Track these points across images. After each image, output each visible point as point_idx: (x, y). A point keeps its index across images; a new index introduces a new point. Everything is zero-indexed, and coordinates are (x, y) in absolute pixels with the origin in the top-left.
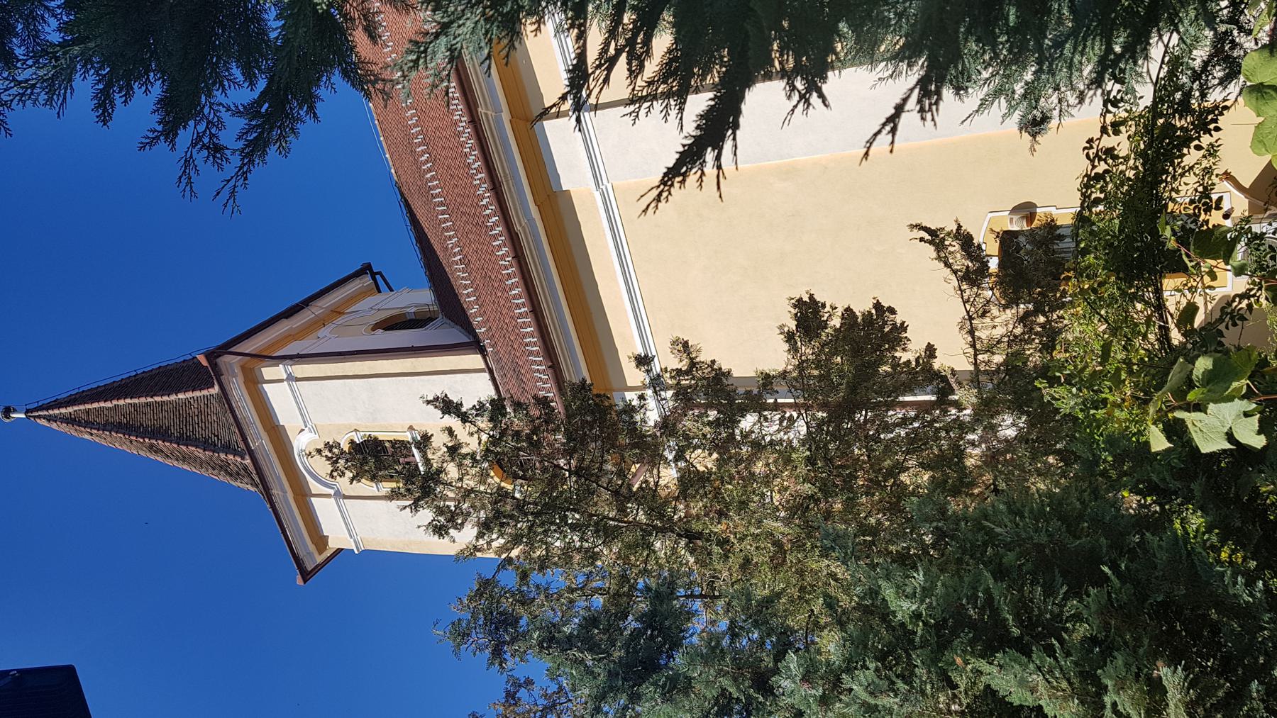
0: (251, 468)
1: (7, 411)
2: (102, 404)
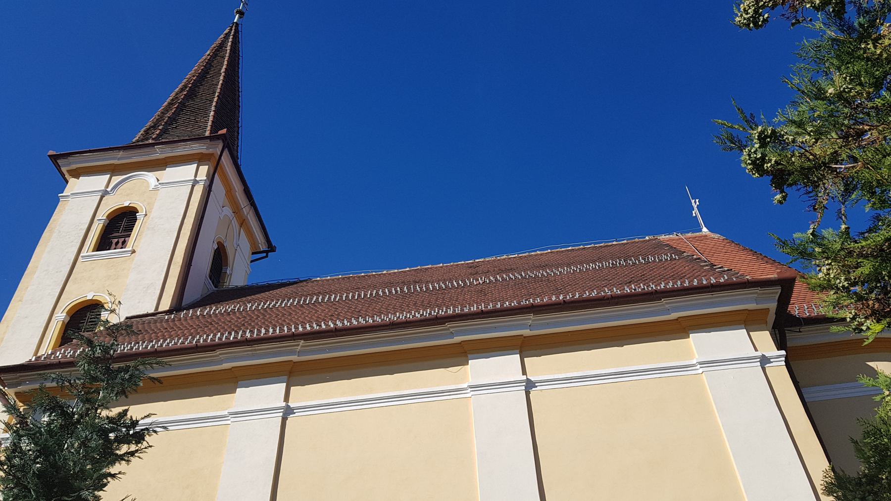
0: (147, 142)
1: (241, 13)
2: (224, 67)
